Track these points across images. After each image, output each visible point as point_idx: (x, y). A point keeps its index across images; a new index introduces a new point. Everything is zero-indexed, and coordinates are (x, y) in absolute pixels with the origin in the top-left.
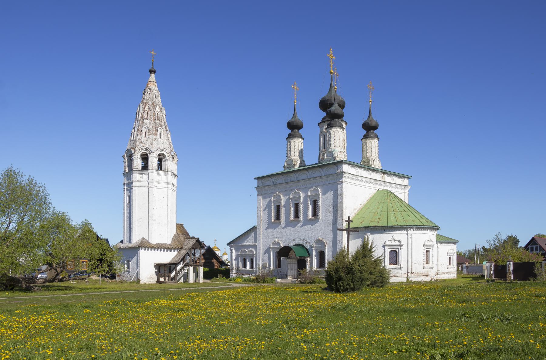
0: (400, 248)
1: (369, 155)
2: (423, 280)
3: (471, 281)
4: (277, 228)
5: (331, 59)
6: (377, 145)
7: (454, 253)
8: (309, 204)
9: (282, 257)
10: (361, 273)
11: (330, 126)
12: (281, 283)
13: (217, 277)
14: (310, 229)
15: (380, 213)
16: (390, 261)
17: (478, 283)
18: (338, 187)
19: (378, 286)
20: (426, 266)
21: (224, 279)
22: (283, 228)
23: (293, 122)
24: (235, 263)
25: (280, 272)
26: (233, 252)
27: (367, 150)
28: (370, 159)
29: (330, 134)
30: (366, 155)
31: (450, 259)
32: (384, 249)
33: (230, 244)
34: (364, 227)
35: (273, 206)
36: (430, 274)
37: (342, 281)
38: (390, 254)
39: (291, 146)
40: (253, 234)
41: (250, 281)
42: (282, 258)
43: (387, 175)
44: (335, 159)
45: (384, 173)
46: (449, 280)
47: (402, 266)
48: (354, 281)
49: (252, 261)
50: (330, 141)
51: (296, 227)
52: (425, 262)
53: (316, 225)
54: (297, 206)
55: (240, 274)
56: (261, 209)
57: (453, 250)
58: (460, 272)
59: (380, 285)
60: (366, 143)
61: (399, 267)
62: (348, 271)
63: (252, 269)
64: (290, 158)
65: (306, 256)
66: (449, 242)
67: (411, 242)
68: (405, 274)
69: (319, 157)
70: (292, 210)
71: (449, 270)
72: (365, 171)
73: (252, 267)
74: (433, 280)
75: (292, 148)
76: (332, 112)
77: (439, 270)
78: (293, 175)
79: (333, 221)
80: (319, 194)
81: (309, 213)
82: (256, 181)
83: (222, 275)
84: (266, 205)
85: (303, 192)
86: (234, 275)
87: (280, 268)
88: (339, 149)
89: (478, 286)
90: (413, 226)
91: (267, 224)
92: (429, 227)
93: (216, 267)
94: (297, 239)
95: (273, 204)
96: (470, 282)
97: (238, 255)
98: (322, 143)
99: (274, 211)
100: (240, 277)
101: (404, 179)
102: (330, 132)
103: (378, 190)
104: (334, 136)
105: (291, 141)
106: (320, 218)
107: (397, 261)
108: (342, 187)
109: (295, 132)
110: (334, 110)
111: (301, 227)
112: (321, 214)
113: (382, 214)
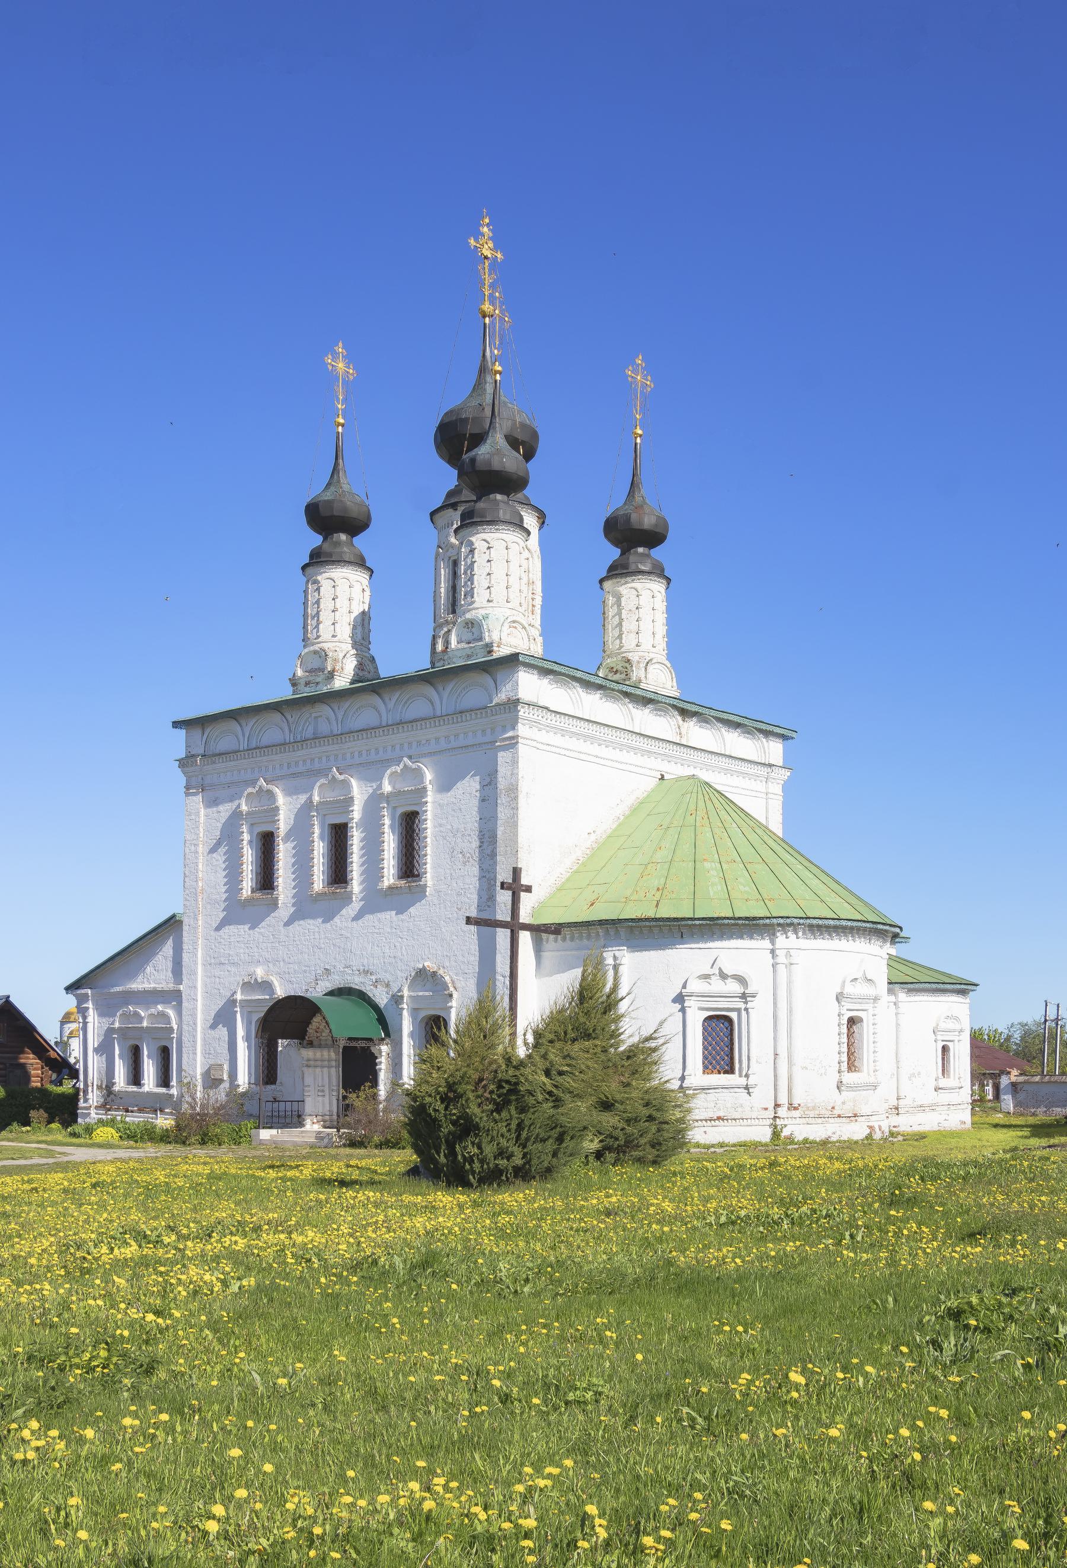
0: (743, 1006)
1: (629, 641)
2: (838, 1133)
3: (1027, 1141)
4: (263, 924)
5: (486, 258)
6: (661, 604)
7: (961, 1031)
8: (387, 829)
9: (280, 1041)
10: (557, 1102)
11: (471, 521)
12: (276, 1145)
13: (26, 1123)
14: (392, 927)
15: (666, 866)
16: (705, 1057)
17: (1050, 1147)
18: (500, 760)
19: (640, 1160)
20: (849, 1078)
21: (50, 1131)
22: (287, 924)
23: (329, 503)
24: (98, 1062)
25: (275, 1100)
26: (90, 1019)
27: (620, 625)
28: (634, 657)
29: (472, 551)
30: (618, 641)
31: (943, 1059)
32: (683, 1010)
33: (78, 988)
34: (602, 923)
35: (246, 837)
36: (863, 1112)
37: (476, 1135)
38: (705, 1029)
39: (319, 600)
40: (168, 948)
41: (151, 1139)
42: (282, 1044)
43: (700, 722)
44: (489, 649)
45: (684, 713)
46: (943, 1135)
47: (751, 1081)
48: (527, 1139)
49: (164, 1056)
50: (471, 579)
51: (337, 919)
52: (846, 1064)
53: (412, 910)
54: (339, 836)
55: (118, 1109)
56: (200, 849)
57: (957, 1019)
58: (990, 1105)
59: (651, 1154)
60: (619, 597)
61: (743, 1081)
62: (499, 1096)
63: (163, 1090)
64: (316, 647)
65: (375, 1038)
66: (942, 986)
67: (790, 983)
68: (766, 1109)
69: (434, 644)
70: (320, 850)
71: (944, 1097)
72: (608, 703)
73: (164, 1080)
74: (877, 1136)
75: (326, 605)
76: (480, 466)
77: (902, 1095)
78: (324, 710)
79: (480, 897)
80: (425, 789)
81: (386, 865)
82: (182, 733)
83: (46, 1115)
84: (219, 833)
85: (365, 779)
86: (93, 1111)
87: (273, 1086)
88: (506, 610)
89: (1048, 1159)
90: (796, 921)
91: (223, 906)
92: (859, 924)
93: (35, 1083)
94: (340, 967)
95: (245, 828)
96: (1022, 1144)
97: (110, 1031)
98: (442, 590)
99: (249, 857)
100: (113, 1120)
101: (764, 740)
102: (472, 543)
103: (662, 778)
104: (489, 561)
105: (319, 578)
106: (429, 883)
107: (732, 1059)
108: (515, 762)
109: (338, 543)
110: (487, 456)
111: (356, 918)
112: (433, 868)
113: (673, 871)
